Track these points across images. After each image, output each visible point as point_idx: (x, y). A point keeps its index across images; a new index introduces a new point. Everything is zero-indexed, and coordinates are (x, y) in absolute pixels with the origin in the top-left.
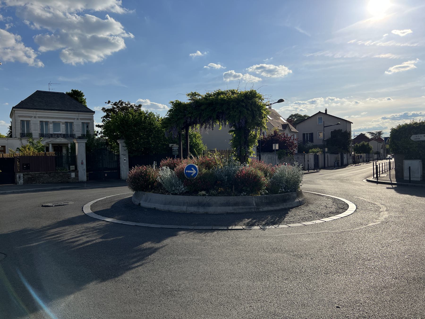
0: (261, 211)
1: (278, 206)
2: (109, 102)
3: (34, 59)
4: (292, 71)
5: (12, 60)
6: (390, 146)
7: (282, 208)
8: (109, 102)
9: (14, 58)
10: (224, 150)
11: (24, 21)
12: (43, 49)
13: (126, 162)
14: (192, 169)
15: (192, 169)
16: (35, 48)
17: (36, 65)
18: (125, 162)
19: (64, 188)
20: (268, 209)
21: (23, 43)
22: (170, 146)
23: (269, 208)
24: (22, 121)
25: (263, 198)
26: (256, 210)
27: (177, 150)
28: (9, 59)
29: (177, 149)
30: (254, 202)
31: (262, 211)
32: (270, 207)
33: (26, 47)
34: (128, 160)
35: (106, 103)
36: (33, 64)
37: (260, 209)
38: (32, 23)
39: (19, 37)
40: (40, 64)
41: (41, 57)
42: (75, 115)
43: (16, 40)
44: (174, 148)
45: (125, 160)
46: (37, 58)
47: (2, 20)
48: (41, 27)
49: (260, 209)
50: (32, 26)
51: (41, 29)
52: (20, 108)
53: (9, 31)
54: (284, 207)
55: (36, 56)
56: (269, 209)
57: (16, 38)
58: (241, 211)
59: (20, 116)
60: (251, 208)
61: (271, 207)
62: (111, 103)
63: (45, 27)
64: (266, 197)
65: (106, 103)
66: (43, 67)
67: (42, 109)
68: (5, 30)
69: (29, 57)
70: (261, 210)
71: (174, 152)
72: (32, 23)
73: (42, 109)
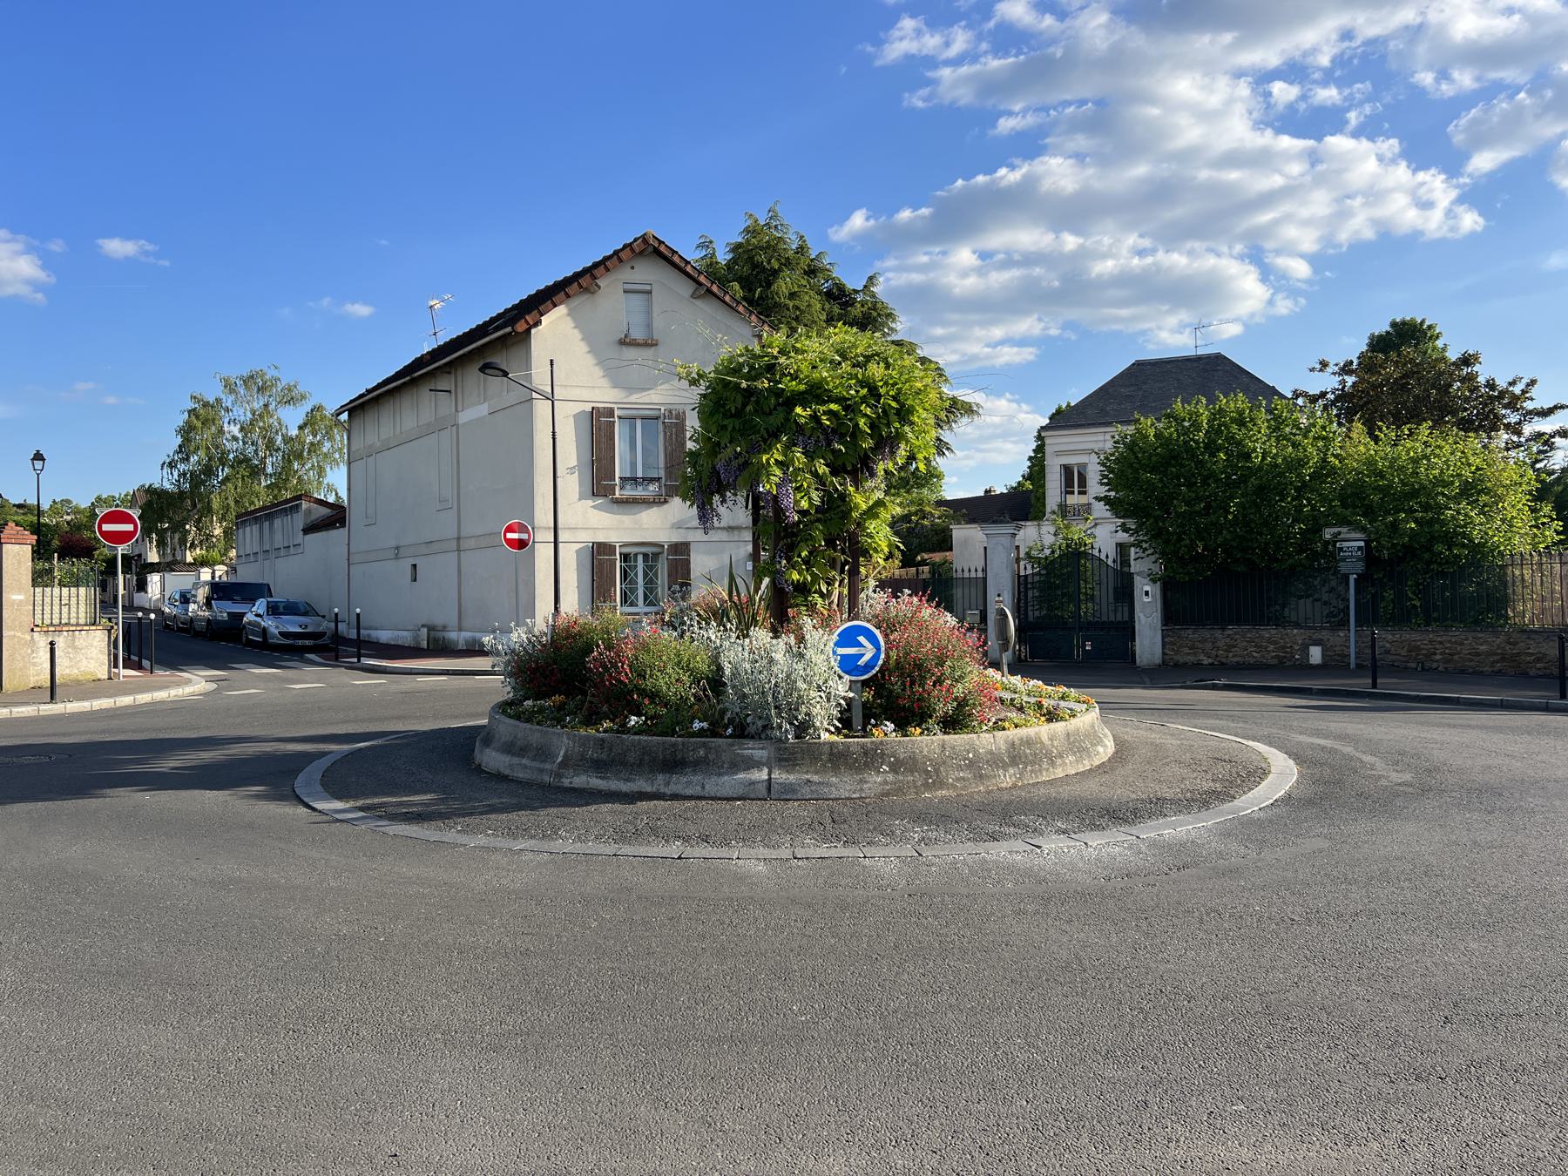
0: (565, 785)
1: (628, 780)
2: (1324, 365)
3: (1153, 256)
4: (1400, 143)
5: (1369, 234)
6: (1413, 534)
7: (643, 790)
8: (1324, 365)
9: (1375, 222)
10: (966, 570)
11: (1417, 76)
12: (1484, 161)
13: (1149, 600)
14: (861, 639)
15: (861, 639)
16: (1452, 165)
17: (1453, 229)
18: (1145, 600)
19: (413, 671)
20: (588, 783)
21: (1404, 164)
22: (1328, 536)
23: (591, 780)
24: (1067, 470)
25: (592, 742)
26: (554, 779)
27: (1359, 553)
28: (1357, 232)
29: (1360, 548)
30: (562, 753)
31: (566, 788)
32: (597, 777)
33: (1415, 171)
34: (1158, 592)
35: (1312, 370)
36: (1439, 228)
37: (564, 780)
38: (1443, 75)
39: (1391, 145)
40: (1470, 220)
41: (1475, 196)
42: (1095, 439)
43: (1380, 158)
44: (1346, 544)
45: (1147, 593)
46: (1460, 200)
47: (1339, 102)
48: (1478, 79)
49: (564, 780)
50: (1444, 87)
51: (1476, 85)
52: (1068, 426)
53: (1356, 134)
54: (654, 790)
55: (1454, 194)
56: (591, 786)
57: (1380, 152)
58: (521, 775)
59: (1058, 454)
60: (541, 771)
61: (601, 778)
62: (1329, 370)
63: (1494, 75)
64: (603, 740)
65: (1312, 370)
66: (1479, 229)
67: (1089, 424)
68: (1346, 135)
69: (1426, 205)
70: (566, 782)
71: (1344, 559)
72: (1443, 75)
73: (1089, 424)
